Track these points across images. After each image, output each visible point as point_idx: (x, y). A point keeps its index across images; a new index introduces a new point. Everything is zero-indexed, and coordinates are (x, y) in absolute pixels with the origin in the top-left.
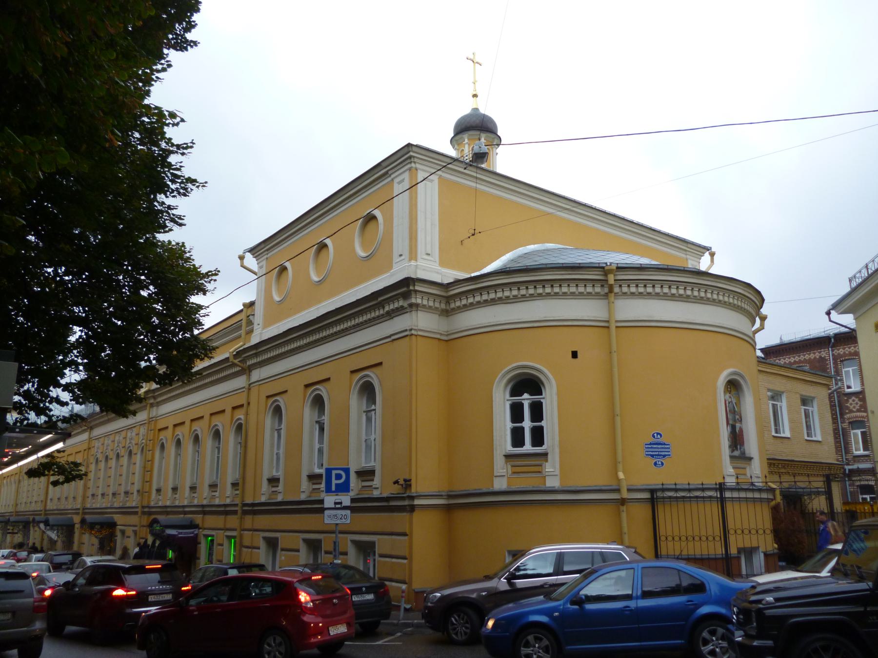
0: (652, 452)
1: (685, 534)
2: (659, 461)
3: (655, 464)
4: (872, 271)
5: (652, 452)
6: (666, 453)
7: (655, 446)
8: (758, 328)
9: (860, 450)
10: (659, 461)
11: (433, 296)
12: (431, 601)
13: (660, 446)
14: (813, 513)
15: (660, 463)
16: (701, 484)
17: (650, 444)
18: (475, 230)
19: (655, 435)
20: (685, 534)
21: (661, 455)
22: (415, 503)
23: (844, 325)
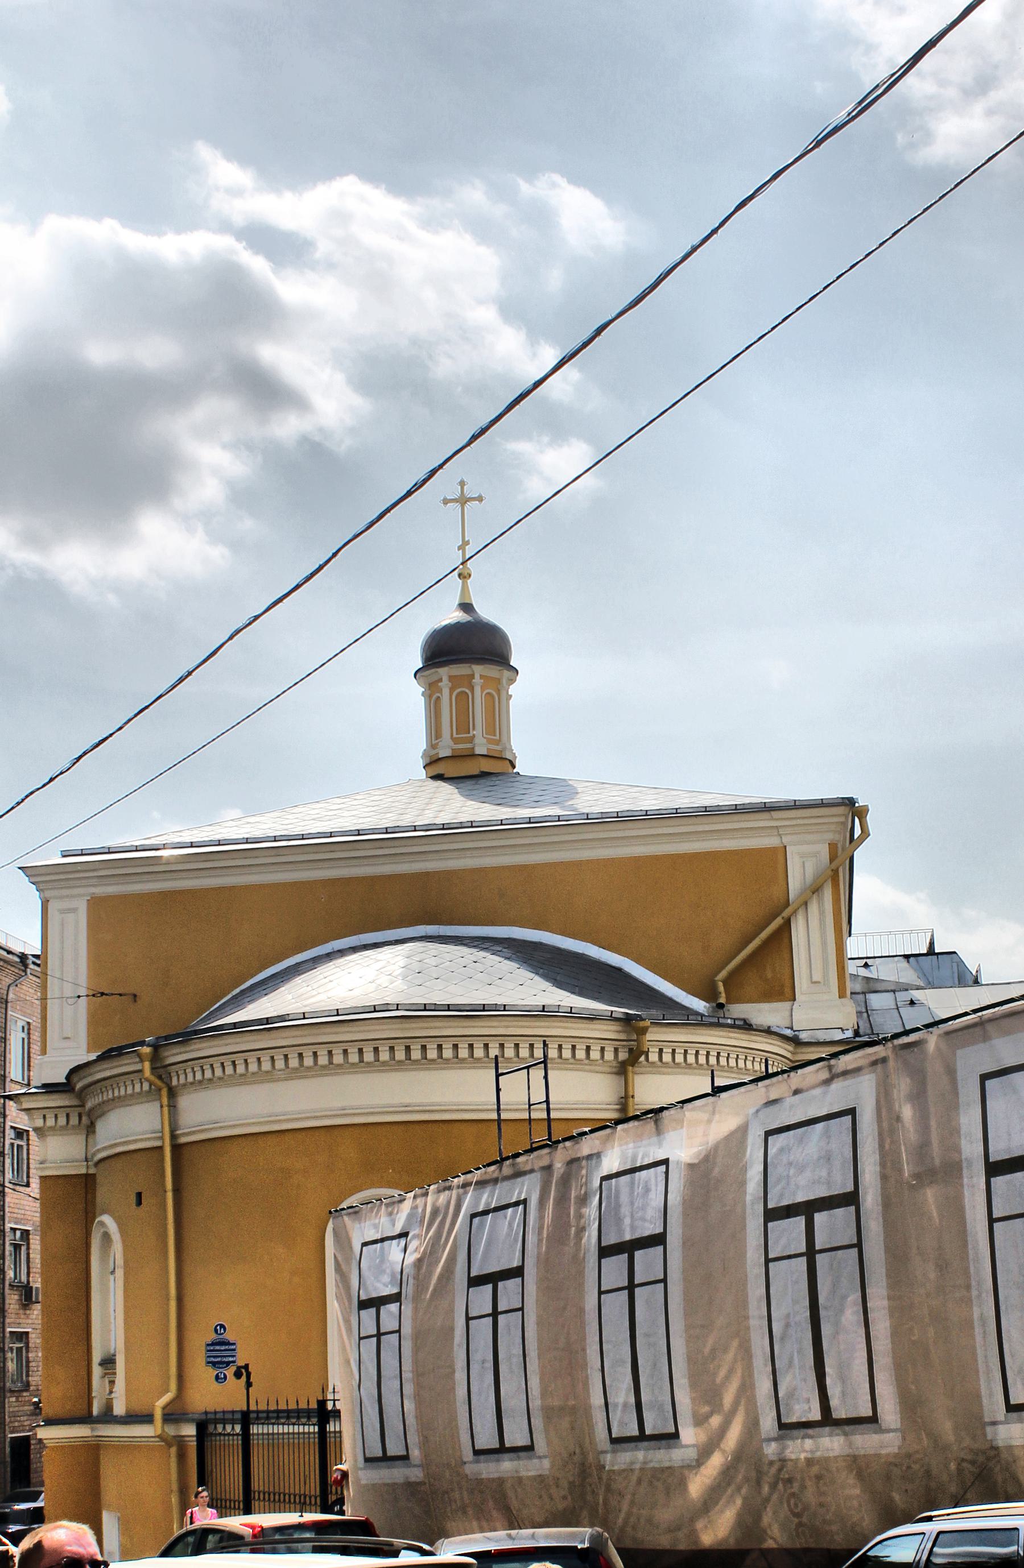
0: (214, 1357)
1: (297, 1506)
2: (221, 1373)
3: (217, 1378)
4: (39, 1044)
5: (214, 1357)
6: (231, 1359)
7: (218, 1348)
8: (963, 1046)
9: (17, 1348)
10: (221, 1373)
11: (52, 1110)
12: (87, 1561)
13: (223, 1348)
14: (780, 1525)
15: (222, 1376)
16: (203, 1413)
17: (213, 1344)
18: (79, 997)
19: (218, 1328)
20: (297, 1506)
21: (224, 1362)
22: (183, 1433)
23: (544, 1081)
